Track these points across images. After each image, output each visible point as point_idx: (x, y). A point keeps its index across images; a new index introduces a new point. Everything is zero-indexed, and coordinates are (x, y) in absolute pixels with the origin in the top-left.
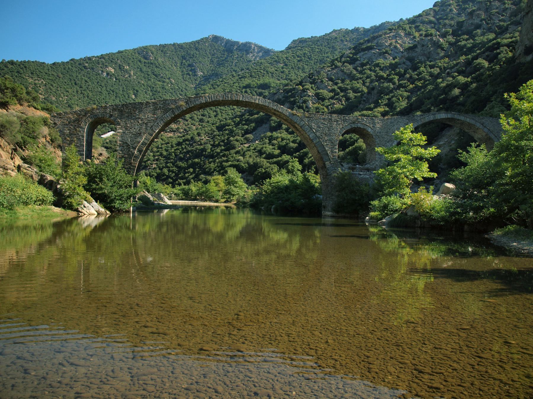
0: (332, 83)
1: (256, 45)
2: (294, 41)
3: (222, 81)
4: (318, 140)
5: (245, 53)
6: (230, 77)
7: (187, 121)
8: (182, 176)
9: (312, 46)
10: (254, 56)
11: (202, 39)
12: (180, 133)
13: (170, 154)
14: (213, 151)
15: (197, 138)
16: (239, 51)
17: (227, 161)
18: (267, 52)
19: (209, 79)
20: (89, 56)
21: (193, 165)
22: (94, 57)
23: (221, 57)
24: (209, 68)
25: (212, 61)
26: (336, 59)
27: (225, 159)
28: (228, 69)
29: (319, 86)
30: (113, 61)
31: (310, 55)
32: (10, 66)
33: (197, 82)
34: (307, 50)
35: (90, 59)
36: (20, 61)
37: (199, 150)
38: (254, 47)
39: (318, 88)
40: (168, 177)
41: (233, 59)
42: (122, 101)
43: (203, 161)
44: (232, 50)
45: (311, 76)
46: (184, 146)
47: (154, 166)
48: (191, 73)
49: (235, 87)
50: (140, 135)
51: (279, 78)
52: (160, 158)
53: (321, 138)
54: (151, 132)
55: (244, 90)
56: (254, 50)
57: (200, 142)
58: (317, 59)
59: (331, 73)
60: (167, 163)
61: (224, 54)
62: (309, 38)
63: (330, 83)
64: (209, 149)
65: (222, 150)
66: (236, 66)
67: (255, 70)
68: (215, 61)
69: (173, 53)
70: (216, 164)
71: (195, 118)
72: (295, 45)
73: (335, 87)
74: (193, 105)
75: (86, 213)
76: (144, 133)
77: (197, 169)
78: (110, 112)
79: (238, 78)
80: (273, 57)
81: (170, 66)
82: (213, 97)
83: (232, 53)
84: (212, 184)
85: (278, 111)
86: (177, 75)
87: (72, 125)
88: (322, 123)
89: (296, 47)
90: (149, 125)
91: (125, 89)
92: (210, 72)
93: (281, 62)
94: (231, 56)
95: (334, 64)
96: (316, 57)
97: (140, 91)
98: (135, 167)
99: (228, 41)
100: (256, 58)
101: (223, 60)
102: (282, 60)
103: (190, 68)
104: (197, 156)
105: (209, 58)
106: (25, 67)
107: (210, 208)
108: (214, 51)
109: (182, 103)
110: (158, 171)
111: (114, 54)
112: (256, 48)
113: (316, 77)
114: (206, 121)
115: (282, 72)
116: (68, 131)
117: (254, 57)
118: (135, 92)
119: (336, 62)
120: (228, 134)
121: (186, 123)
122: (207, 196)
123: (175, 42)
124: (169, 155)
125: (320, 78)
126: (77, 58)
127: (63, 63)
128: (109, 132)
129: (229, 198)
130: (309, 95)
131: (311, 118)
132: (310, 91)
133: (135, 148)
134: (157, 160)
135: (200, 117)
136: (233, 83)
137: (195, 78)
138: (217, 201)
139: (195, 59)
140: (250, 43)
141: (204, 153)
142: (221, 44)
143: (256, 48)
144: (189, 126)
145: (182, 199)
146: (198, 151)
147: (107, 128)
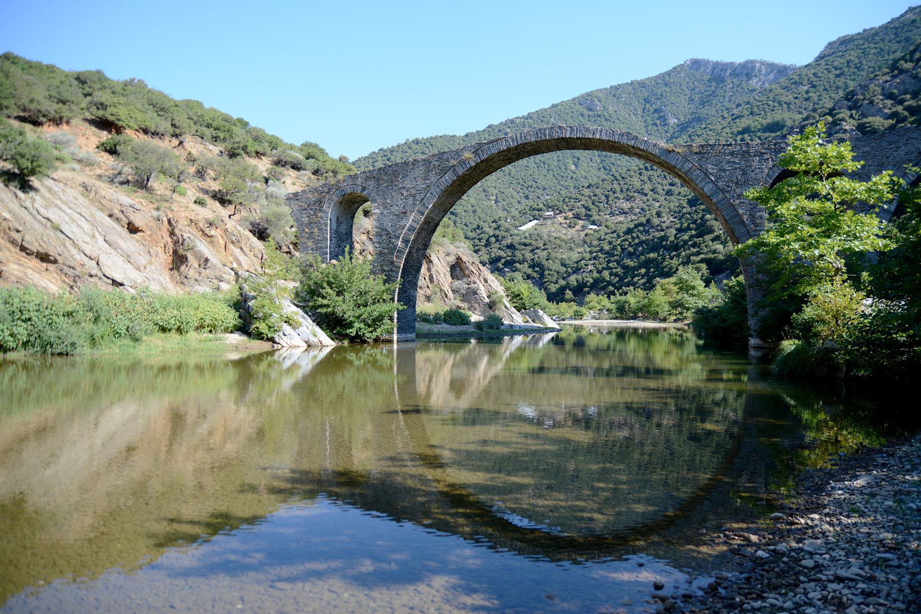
0: (892, 102)
1: (762, 63)
2: (830, 44)
3: (705, 128)
4: (721, 196)
5: (744, 78)
6: (719, 120)
7: (646, 195)
8: (629, 281)
9: (863, 47)
10: (760, 80)
11: (675, 68)
12: (635, 215)
13: (614, 248)
14: (678, 238)
15: (656, 221)
16: (734, 78)
17: (698, 253)
18: (782, 70)
19: (687, 127)
20: (511, 118)
21: (647, 264)
22: (518, 118)
23: (706, 91)
24: (687, 110)
25: (692, 100)
26: (903, 58)
27: (695, 250)
28: (718, 108)
29: (865, 112)
30: (544, 119)
31: (861, 63)
32: (414, 146)
33: (669, 135)
34: (853, 56)
35: (512, 121)
36: (426, 138)
37: (658, 239)
38: (761, 67)
39: (865, 116)
40: (610, 283)
41: (725, 92)
42: (556, 175)
43: (662, 255)
44: (724, 78)
45: (850, 96)
46: (634, 235)
47: (590, 267)
48: (658, 122)
49: (725, 135)
50: (404, 216)
51: (800, 110)
52: (600, 254)
53: (728, 192)
54: (422, 209)
55: (739, 137)
56: (760, 71)
57: (661, 226)
58: (874, 67)
59: (891, 85)
60: (609, 262)
61: (710, 86)
62: (859, 34)
63: (889, 102)
64: (673, 237)
65: (691, 237)
66: (730, 101)
67: (758, 103)
68: (697, 98)
69: (631, 96)
70: (681, 260)
71: (659, 189)
72: (832, 50)
73: (900, 108)
74: (486, 157)
75: (285, 344)
76: (412, 212)
77: (652, 270)
78: (362, 182)
79: (730, 119)
80: (792, 76)
81: (627, 116)
82: (519, 137)
83: (722, 82)
84: (658, 291)
85: (639, 149)
86: (638, 127)
87: (311, 209)
88: (728, 162)
89: (833, 53)
90: (418, 197)
91: (561, 158)
92: (689, 117)
93: (805, 82)
94: (722, 87)
95: (897, 68)
96: (872, 64)
97: (582, 158)
98: (399, 268)
99: (716, 65)
100: (764, 83)
101: (709, 96)
102: (806, 79)
103: (656, 115)
104: (654, 249)
105: (686, 95)
106: (431, 145)
107: (656, 332)
108: (693, 83)
109: (467, 155)
110: (596, 275)
111: (545, 110)
112: (763, 67)
113: (859, 97)
114: (677, 192)
115: (806, 100)
116: (307, 219)
117: (760, 83)
118: (576, 160)
119: (902, 62)
120: (703, 210)
121: (645, 198)
122: (647, 312)
123: (633, 79)
124: (613, 249)
125: (868, 97)
126: (496, 122)
127: (478, 132)
128: (530, 221)
129: (681, 313)
130: (846, 130)
131: (705, 153)
132: (846, 122)
133: (398, 238)
134: (595, 258)
135: (668, 188)
136: (722, 129)
137: (666, 128)
138: (664, 320)
139: (665, 100)
140: (753, 62)
141: (664, 243)
142: (705, 71)
143: (763, 67)
144: (648, 203)
145: (616, 318)
146: (656, 240)
147: (529, 216)
